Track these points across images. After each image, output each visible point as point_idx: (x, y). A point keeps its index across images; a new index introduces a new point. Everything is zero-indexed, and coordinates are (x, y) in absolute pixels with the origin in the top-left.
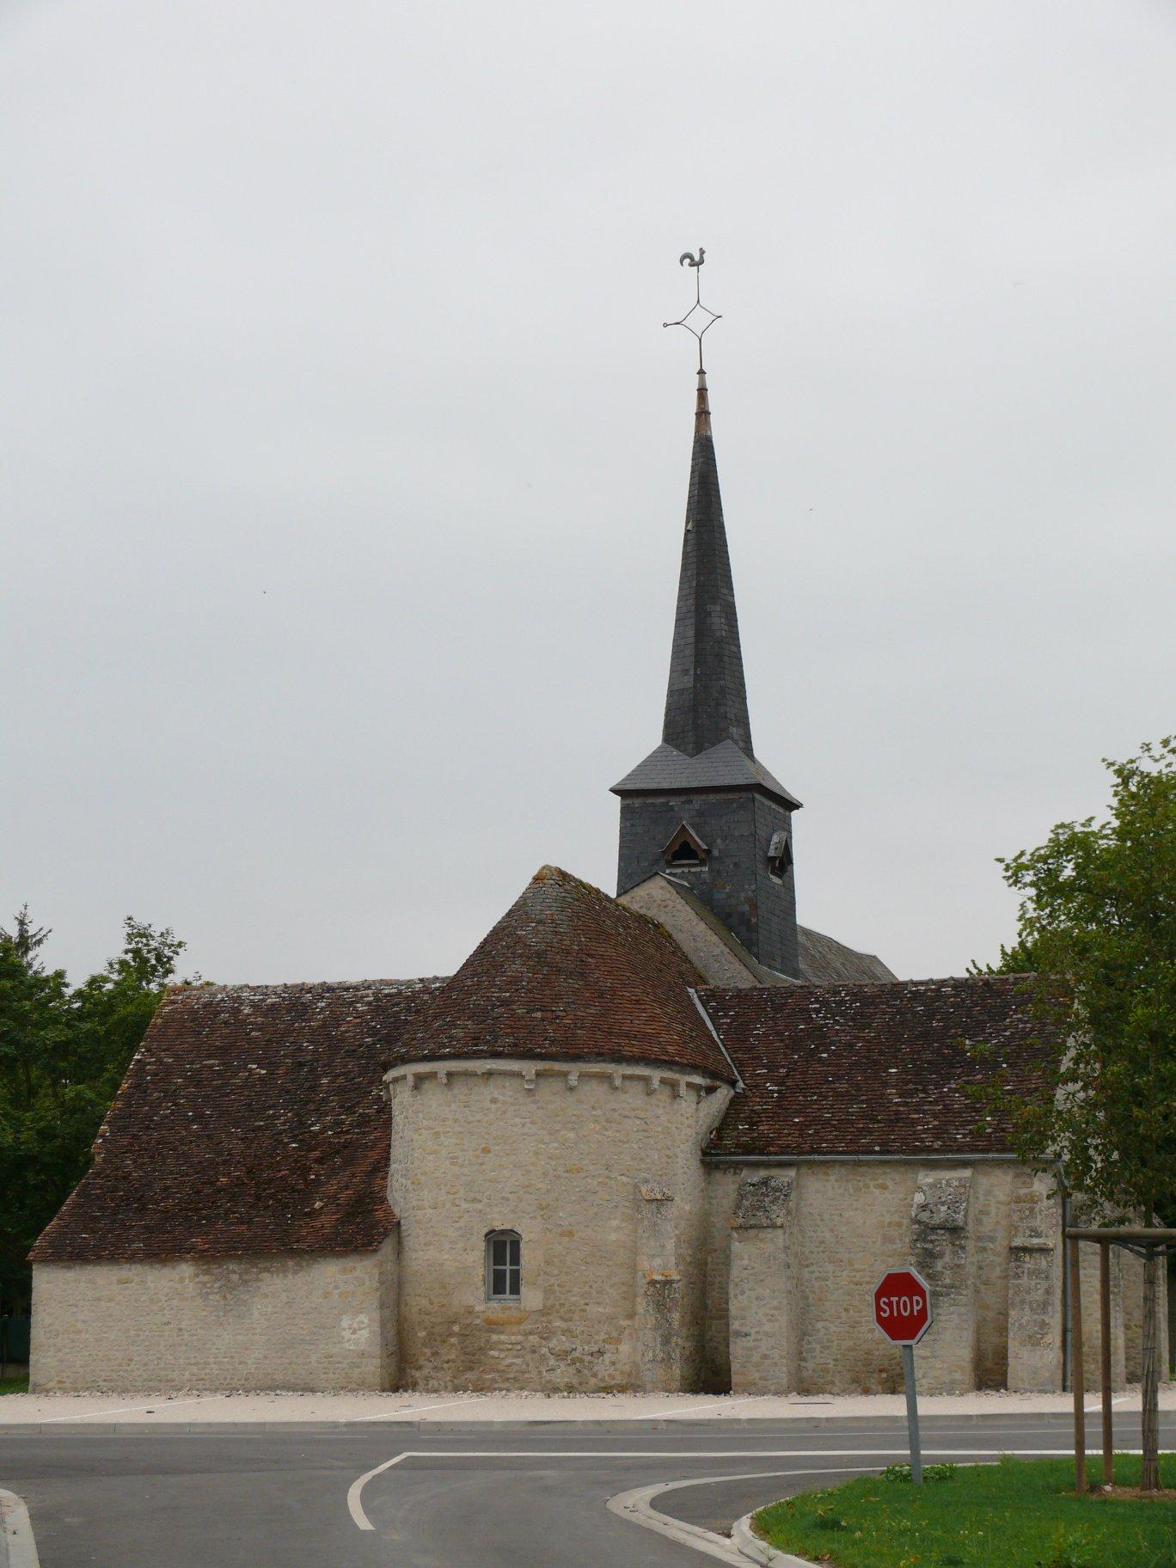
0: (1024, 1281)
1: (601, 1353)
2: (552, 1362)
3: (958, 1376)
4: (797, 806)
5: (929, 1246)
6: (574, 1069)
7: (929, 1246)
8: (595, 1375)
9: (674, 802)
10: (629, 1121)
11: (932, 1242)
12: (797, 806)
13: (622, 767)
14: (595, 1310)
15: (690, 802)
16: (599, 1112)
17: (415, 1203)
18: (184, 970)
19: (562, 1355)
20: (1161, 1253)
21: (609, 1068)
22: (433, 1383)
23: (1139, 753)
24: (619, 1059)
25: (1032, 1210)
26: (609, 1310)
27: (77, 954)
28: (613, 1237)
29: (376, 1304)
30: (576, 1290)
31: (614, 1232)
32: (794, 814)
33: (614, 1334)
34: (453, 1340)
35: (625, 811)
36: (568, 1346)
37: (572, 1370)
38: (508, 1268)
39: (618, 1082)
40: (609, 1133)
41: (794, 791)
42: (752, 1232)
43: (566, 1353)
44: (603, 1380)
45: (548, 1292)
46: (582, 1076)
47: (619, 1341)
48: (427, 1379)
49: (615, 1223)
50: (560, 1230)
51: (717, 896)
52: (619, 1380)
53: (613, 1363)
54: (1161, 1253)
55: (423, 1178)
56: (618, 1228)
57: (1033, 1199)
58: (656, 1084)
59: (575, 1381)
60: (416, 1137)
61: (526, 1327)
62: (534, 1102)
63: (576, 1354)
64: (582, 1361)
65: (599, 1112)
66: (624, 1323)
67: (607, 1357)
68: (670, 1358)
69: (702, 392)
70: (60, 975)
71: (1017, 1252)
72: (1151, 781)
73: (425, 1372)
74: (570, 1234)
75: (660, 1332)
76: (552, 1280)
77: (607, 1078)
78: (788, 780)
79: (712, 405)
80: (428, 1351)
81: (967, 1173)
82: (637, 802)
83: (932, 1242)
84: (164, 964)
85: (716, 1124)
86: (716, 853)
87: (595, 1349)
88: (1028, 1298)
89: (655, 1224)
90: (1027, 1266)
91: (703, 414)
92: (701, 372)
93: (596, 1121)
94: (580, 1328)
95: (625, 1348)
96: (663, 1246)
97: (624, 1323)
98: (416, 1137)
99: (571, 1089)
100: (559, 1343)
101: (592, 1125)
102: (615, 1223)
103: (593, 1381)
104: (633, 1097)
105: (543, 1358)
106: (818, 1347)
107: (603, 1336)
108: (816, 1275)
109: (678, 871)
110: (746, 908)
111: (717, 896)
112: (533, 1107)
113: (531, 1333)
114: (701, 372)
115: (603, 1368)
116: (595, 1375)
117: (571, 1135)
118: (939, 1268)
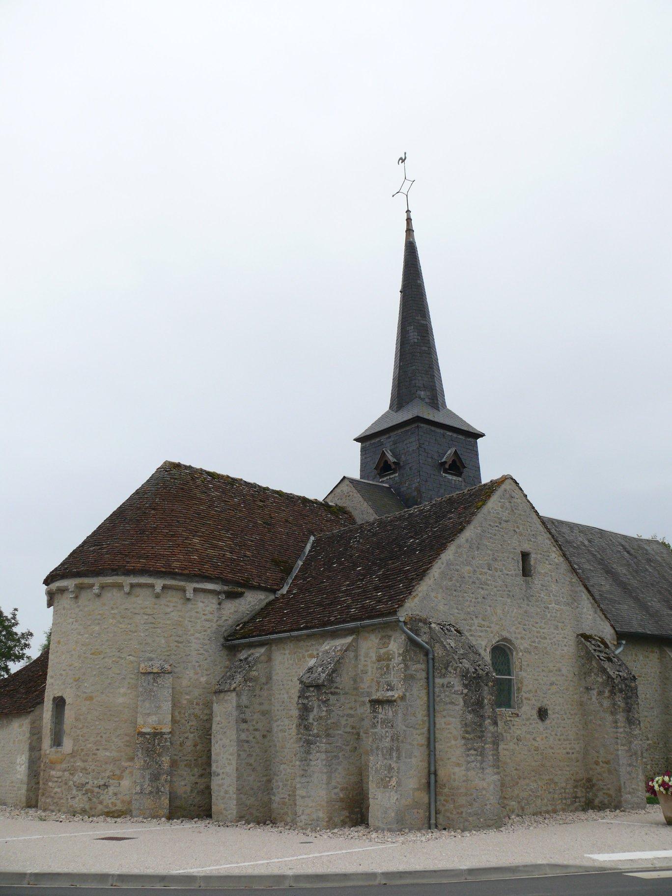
0: (378, 730)
1: (106, 786)
2: (74, 792)
3: (321, 814)
4: (482, 435)
5: (306, 701)
6: (97, 582)
7: (306, 701)
8: (101, 803)
9: (383, 439)
10: (139, 617)
11: (307, 698)
13: (364, 424)
14: (103, 754)
15: (389, 437)
16: (116, 611)
19: (80, 787)
21: (120, 579)
24: (128, 573)
25: (388, 667)
26: (115, 754)
28: (121, 700)
29: (27, 747)
30: (92, 739)
31: (122, 697)
32: (479, 441)
33: (118, 772)
35: (363, 450)
36: (84, 780)
37: (85, 798)
39: (190, 594)
40: (122, 626)
42: (222, 695)
43: (83, 785)
44: (107, 807)
45: (76, 740)
46: (103, 587)
47: (120, 778)
49: (122, 690)
50: (85, 695)
51: (402, 489)
52: (119, 806)
53: (116, 794)
56: (125, 694)
57: (388, 658)
58: (190, 594)
59: (87, 807)
61: (64, 766)
62: (78, 607)
63: (88, 787)
64: (92, 792)
65: (116, 611)
66: (126, 764)
67: (111, 790)
68: (158, 791)
69: (409, 220)
71: (376, 703)
74: (90, 698)
75: (148, 771)
76: (78, 731)
78: (473, 420)
79: (415, 227)
81: (349, 639)
82: (368, 443)
83: (307, 698)
85: (246, 619)
86: (402, 464)
87: (102, 783)
88: (381, 745)
89: (151, 691)
90: (380, 716)
91: (409, 231)
92: (408, 211)
93: (114, 618)
94: (93, 767)
95: (126, 783)
96: (159, 707)
97: (126, 764)
99: (189, 599)
100: (79, 778)
101: (111, 621)
102: (122, 690)
103: (100, 807)
104: (143, 601)
105: (70, 789)
106: (280, 784)
107: (108, 774)
108: (281, 727)
109: (385, 479)
110: (415, 493)
111: (402, 489)
112: (77, 610)
113: (65, 770)
114: (408, 211)
115: (108, 798)
116: (101, 803)
117: (97, 628)
118: (311, 721)
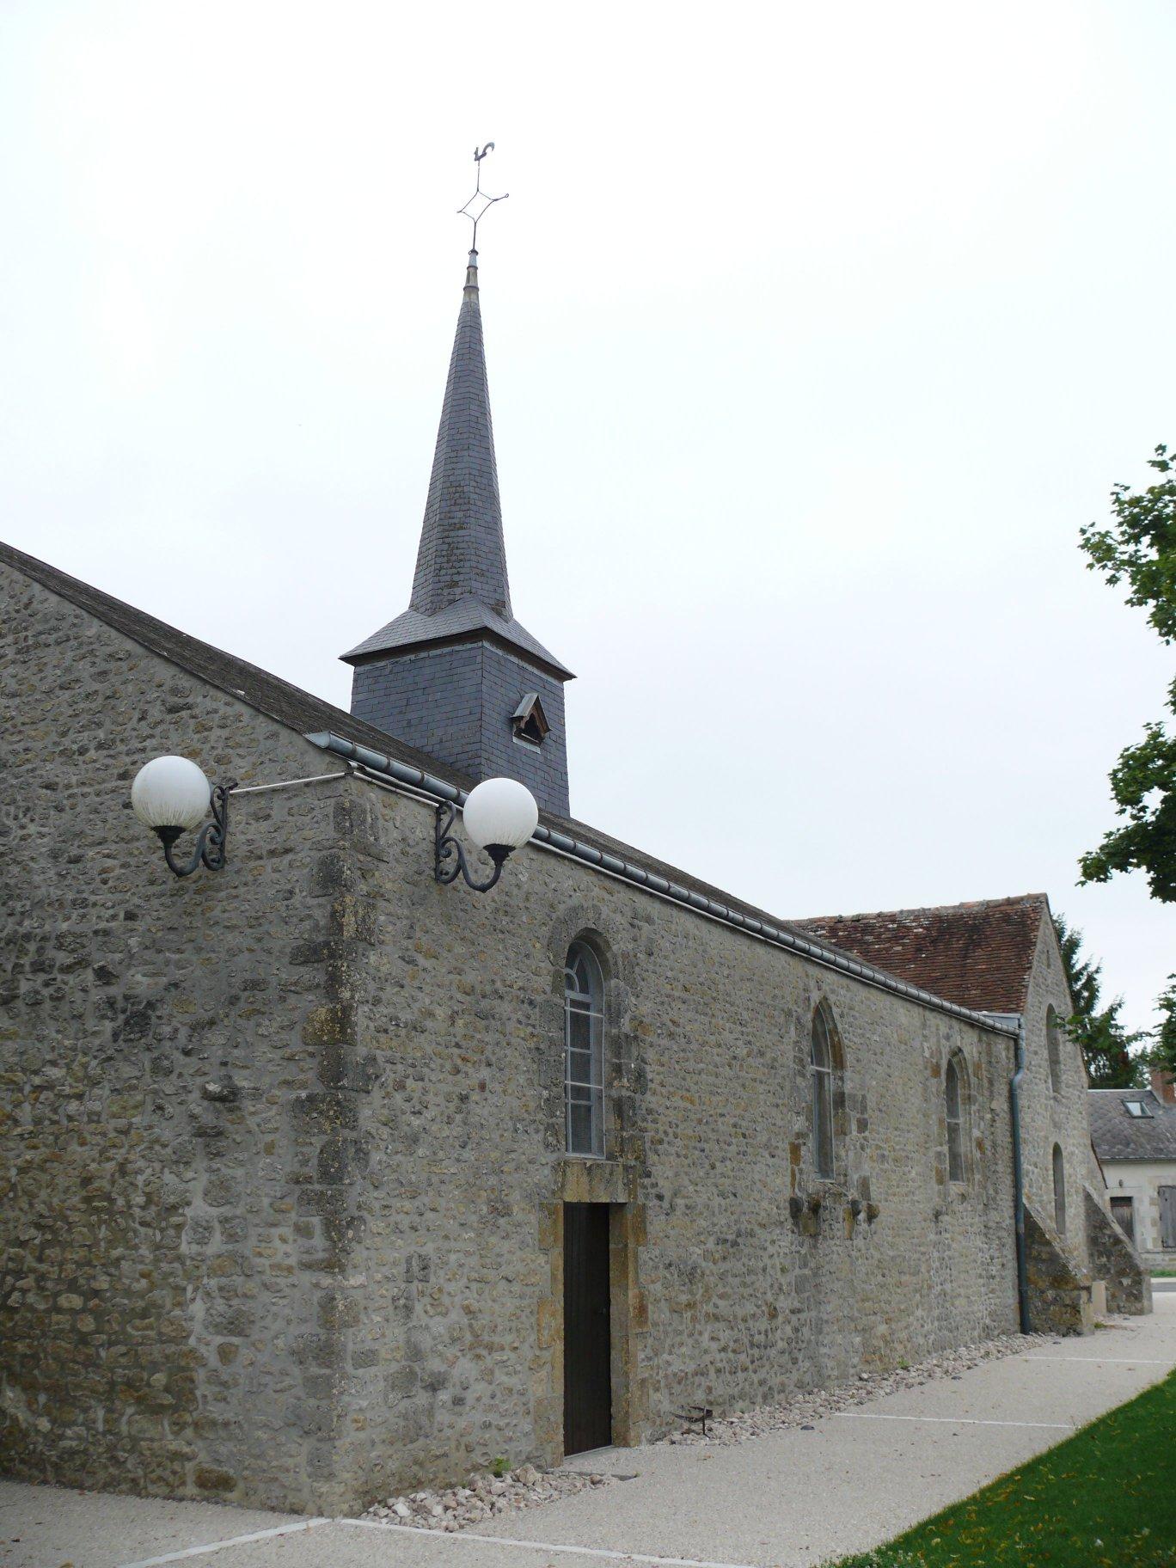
4: (571, 677)
12: (571, 677)
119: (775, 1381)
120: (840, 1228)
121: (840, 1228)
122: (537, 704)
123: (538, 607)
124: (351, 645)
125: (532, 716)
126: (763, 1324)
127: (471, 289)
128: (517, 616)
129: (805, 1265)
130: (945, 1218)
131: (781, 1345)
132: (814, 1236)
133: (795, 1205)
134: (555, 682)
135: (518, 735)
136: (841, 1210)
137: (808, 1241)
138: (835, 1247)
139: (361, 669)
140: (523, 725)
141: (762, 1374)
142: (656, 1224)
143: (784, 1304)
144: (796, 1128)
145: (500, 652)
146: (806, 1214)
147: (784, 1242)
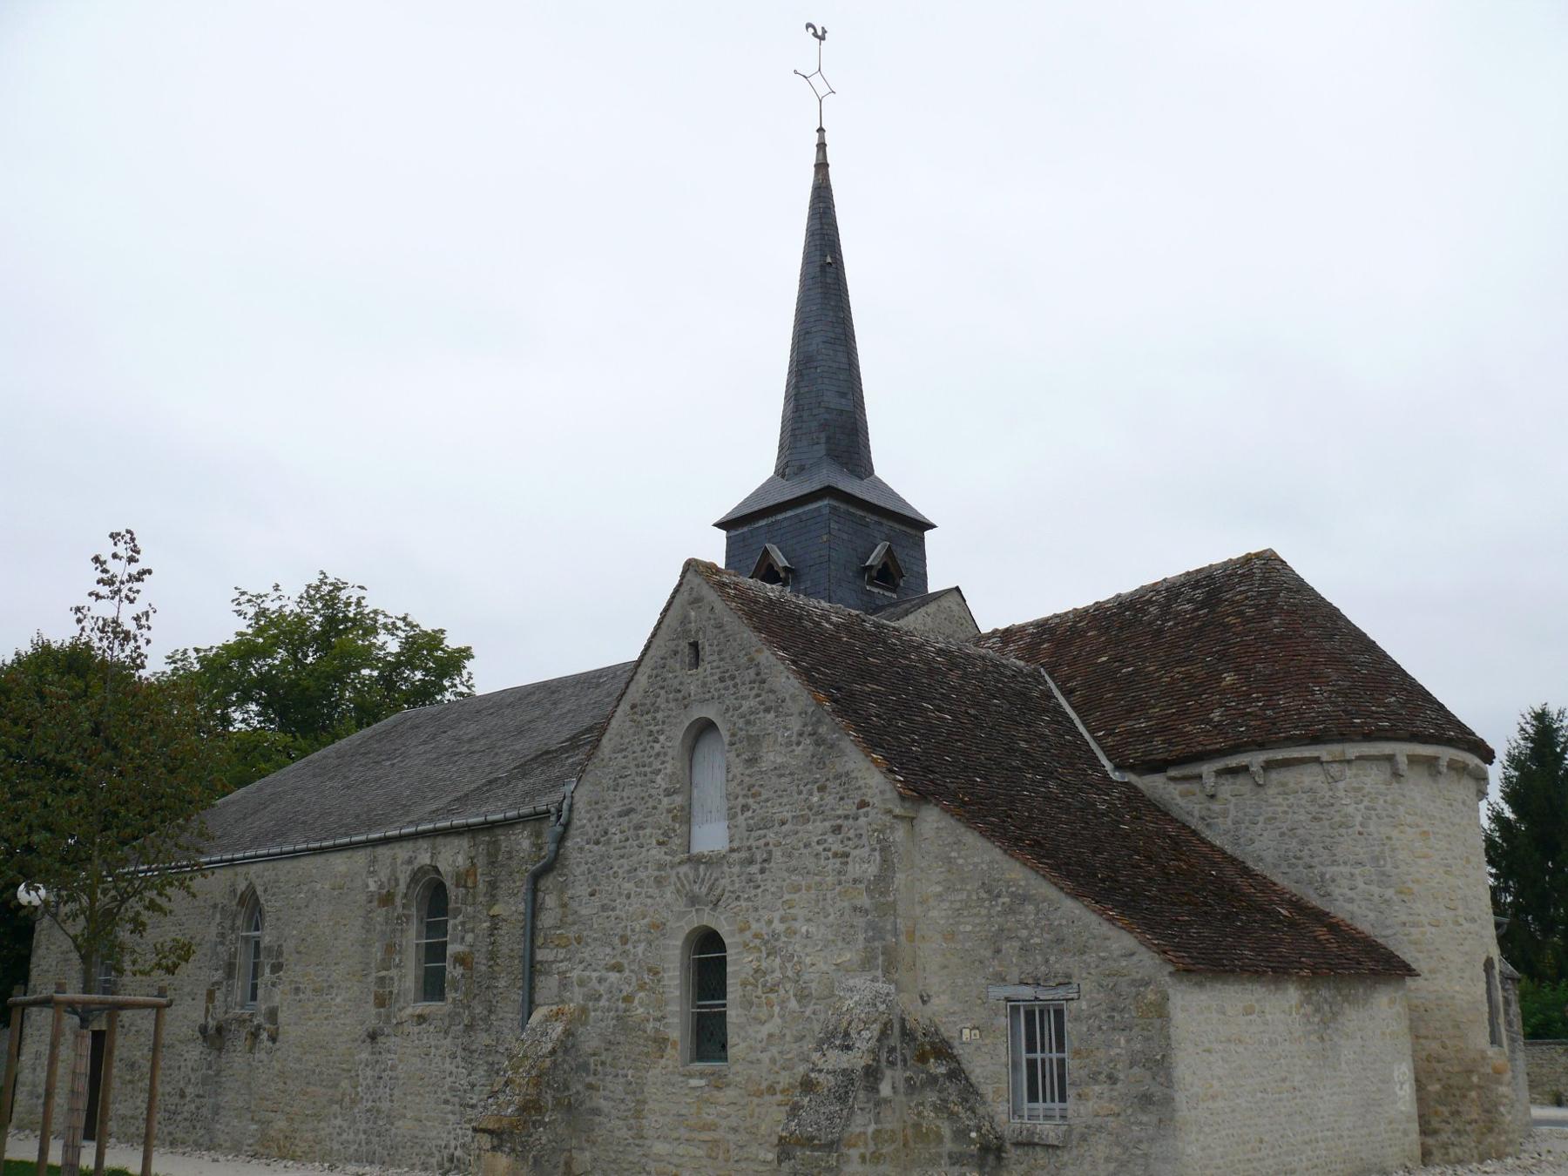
4: (932, 526)
12: (932, 526)
17: (1404, 918)
18: (487, 676)
20: (43, 1152)
22: (1456, 1152)
23: (270, 590)
27: (9, 659)
34: (1473, 1094)
38: (1039, 1056)
41: (925, 510)
48: (1445, 1146)
54: (43, 1152)
55: (1415, 887)
60: (1395, 834)
70: (465, 653)
72: (271, 623)
73: (1444, 1137)
77: (1431, 763)
80: (1445, 1111)
84: (455, 662)
98: (1395, 834)
119: (179, 1135)
120: (241, 1044)
121: (241, 1044)
122: (889, 551)
123: (901, 460)
124: (722, 513)
125: (885, 564)
126: (176, 1099)
127: (822, 167)
128: (879, 472)
129: (210, 1068)
130: (381, 1039)
131: (186, 1115)
132: (220, 1050)
133: (203, 1030)
134: (913, 532)
135: (871, 583)
136: (244, 1033)
137: (215, 1053)
138: (237, 1058)
139: (733, 533)
140: (874, 573)
141: (171, 1128)
142: (119, 1040)
143: (190, 1090)
144: (215, 979)
145: (745, 529)
146: (215, 1037)
147: (194, 1053)
